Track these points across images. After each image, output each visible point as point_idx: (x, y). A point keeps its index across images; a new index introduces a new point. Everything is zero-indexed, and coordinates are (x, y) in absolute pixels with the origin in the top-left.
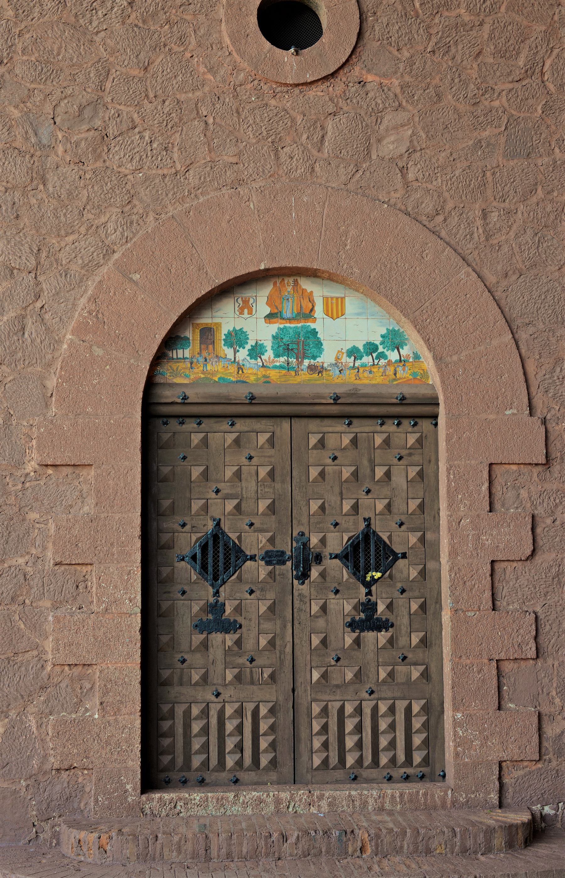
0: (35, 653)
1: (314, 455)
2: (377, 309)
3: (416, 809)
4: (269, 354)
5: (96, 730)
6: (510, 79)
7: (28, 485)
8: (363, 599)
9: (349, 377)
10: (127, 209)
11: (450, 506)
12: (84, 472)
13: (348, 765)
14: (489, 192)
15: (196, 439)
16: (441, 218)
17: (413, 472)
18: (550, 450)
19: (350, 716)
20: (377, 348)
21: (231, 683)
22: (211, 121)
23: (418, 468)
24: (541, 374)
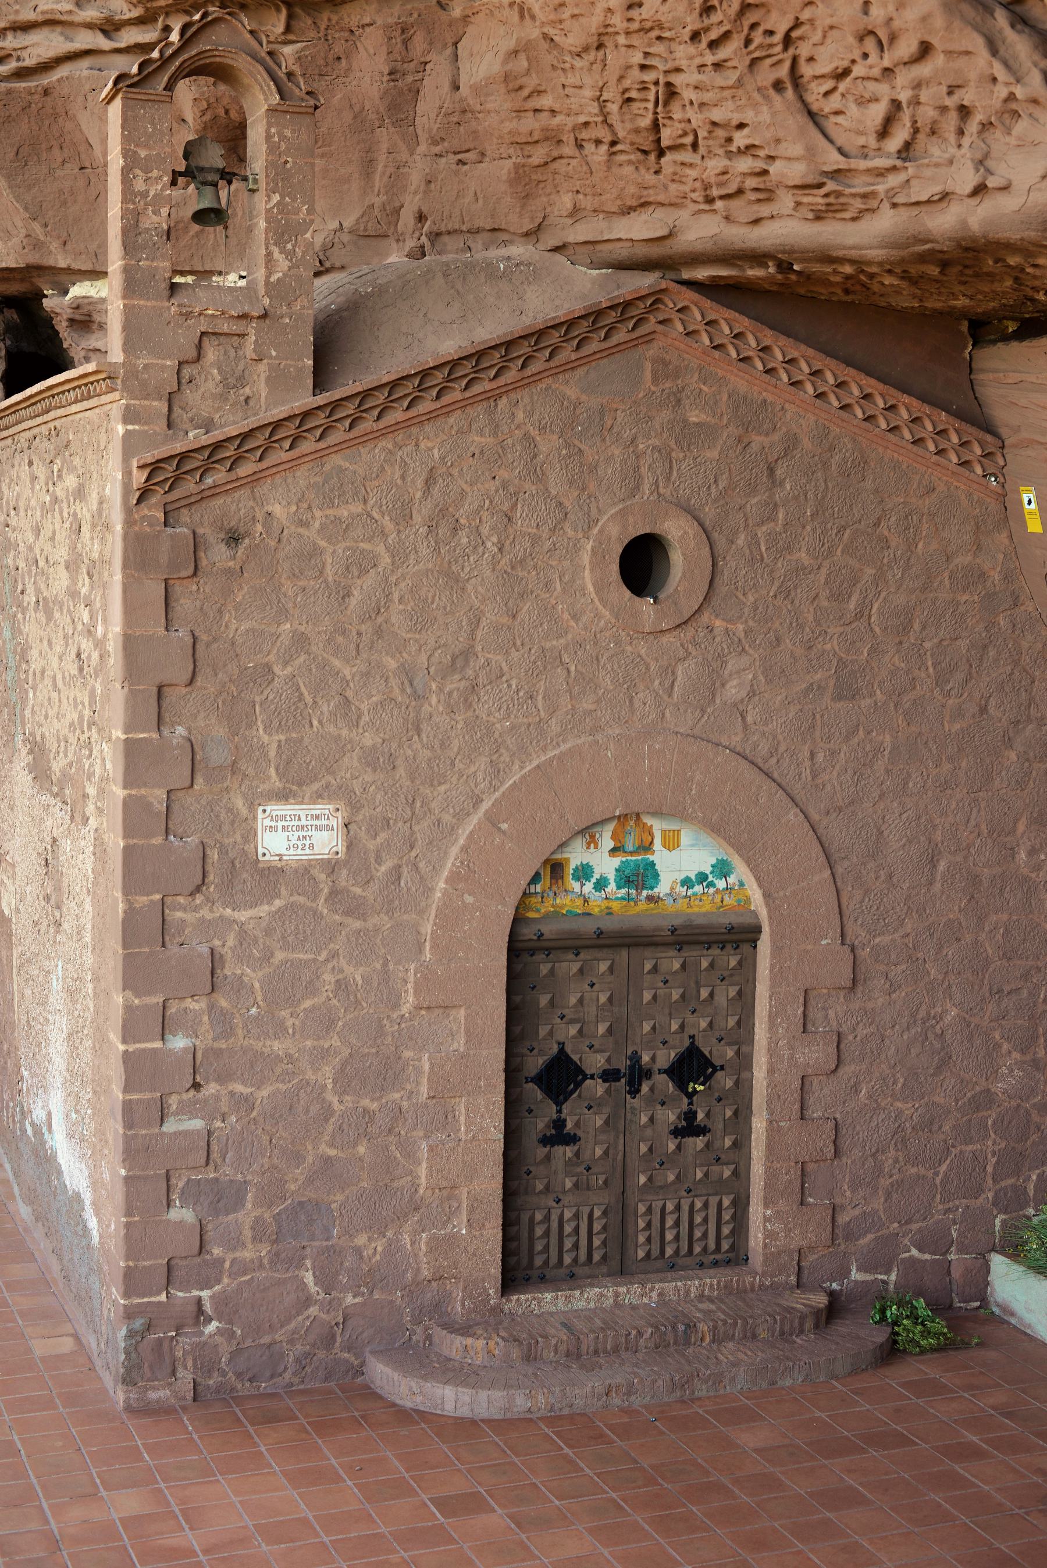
1: (648, 978)
2: (709, 840)
4: (612, 887)
5: (464, 1244)
9: (682, 904)
12: (454, 1012)
13: (667, 1255)
14: (818, 733)
16: (774, 760)
17: (733, 992)
22: (573, 668)
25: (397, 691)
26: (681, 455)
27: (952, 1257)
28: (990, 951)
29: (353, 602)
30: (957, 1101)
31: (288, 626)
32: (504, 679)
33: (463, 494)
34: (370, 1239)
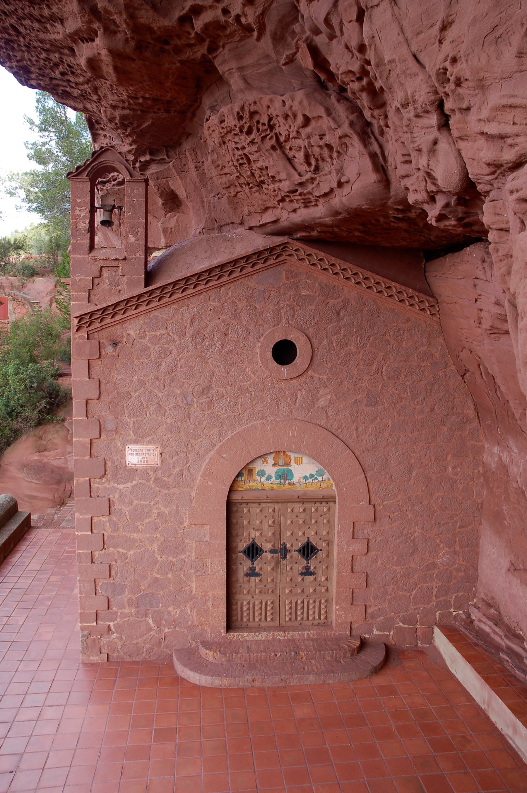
4: (273, 479)
5: (211, 613)
10: (220, 429)
11: (338, 537)
12: (205, 526)
14: (359, 420)
16: (340, 430)
22: (253, 393)
24: (374, 488)
25: (180, 402)
27: (418, 626)
28: (435, 508)
29: (162, 368)
30: (420, 566)
32: (224, 397)
33: (206, 325)
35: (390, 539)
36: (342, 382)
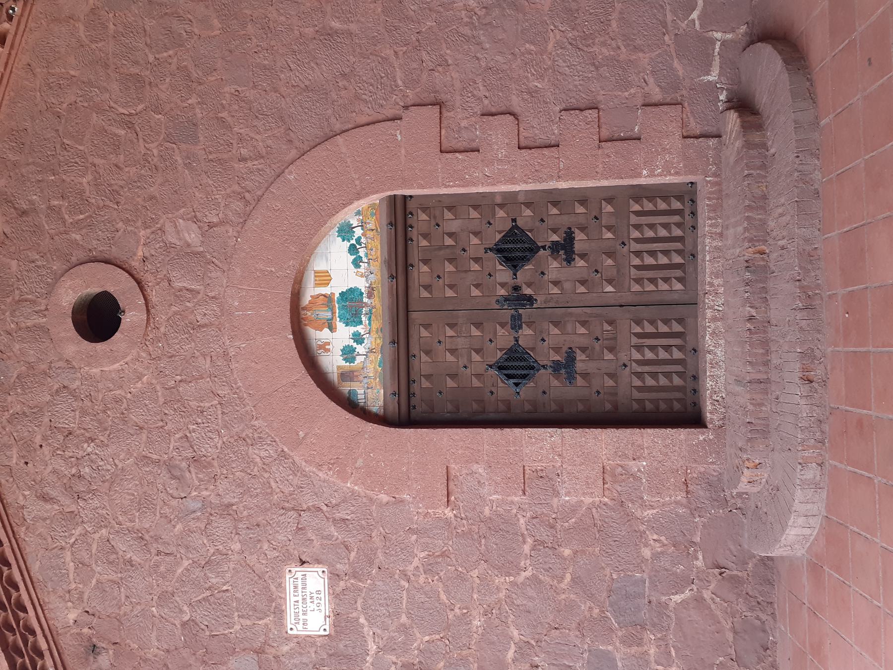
0: (594, 510)
2: (322, 245)
3: (722, 206)
5: (655, 464)
6: (136, 141)
7: (463, 516)
8: (548, 252)
9: (376, 267)
11: (474, 185)
12: (453, 472)
14: (225, 156)
15: (425, 384)
16: (247, 195)
17: (448, 215)
18: (428, 102)
19: (642, 260)
20: (353, 244)
21: (615, 356)
22: (179, 378)
23: (445, 210)
26: (17, 292)
31: (154, 609)
32: (188, 435)
33: (54, 471)
34: (646, 545)
35: (483, 64)
36: (152, 198)
